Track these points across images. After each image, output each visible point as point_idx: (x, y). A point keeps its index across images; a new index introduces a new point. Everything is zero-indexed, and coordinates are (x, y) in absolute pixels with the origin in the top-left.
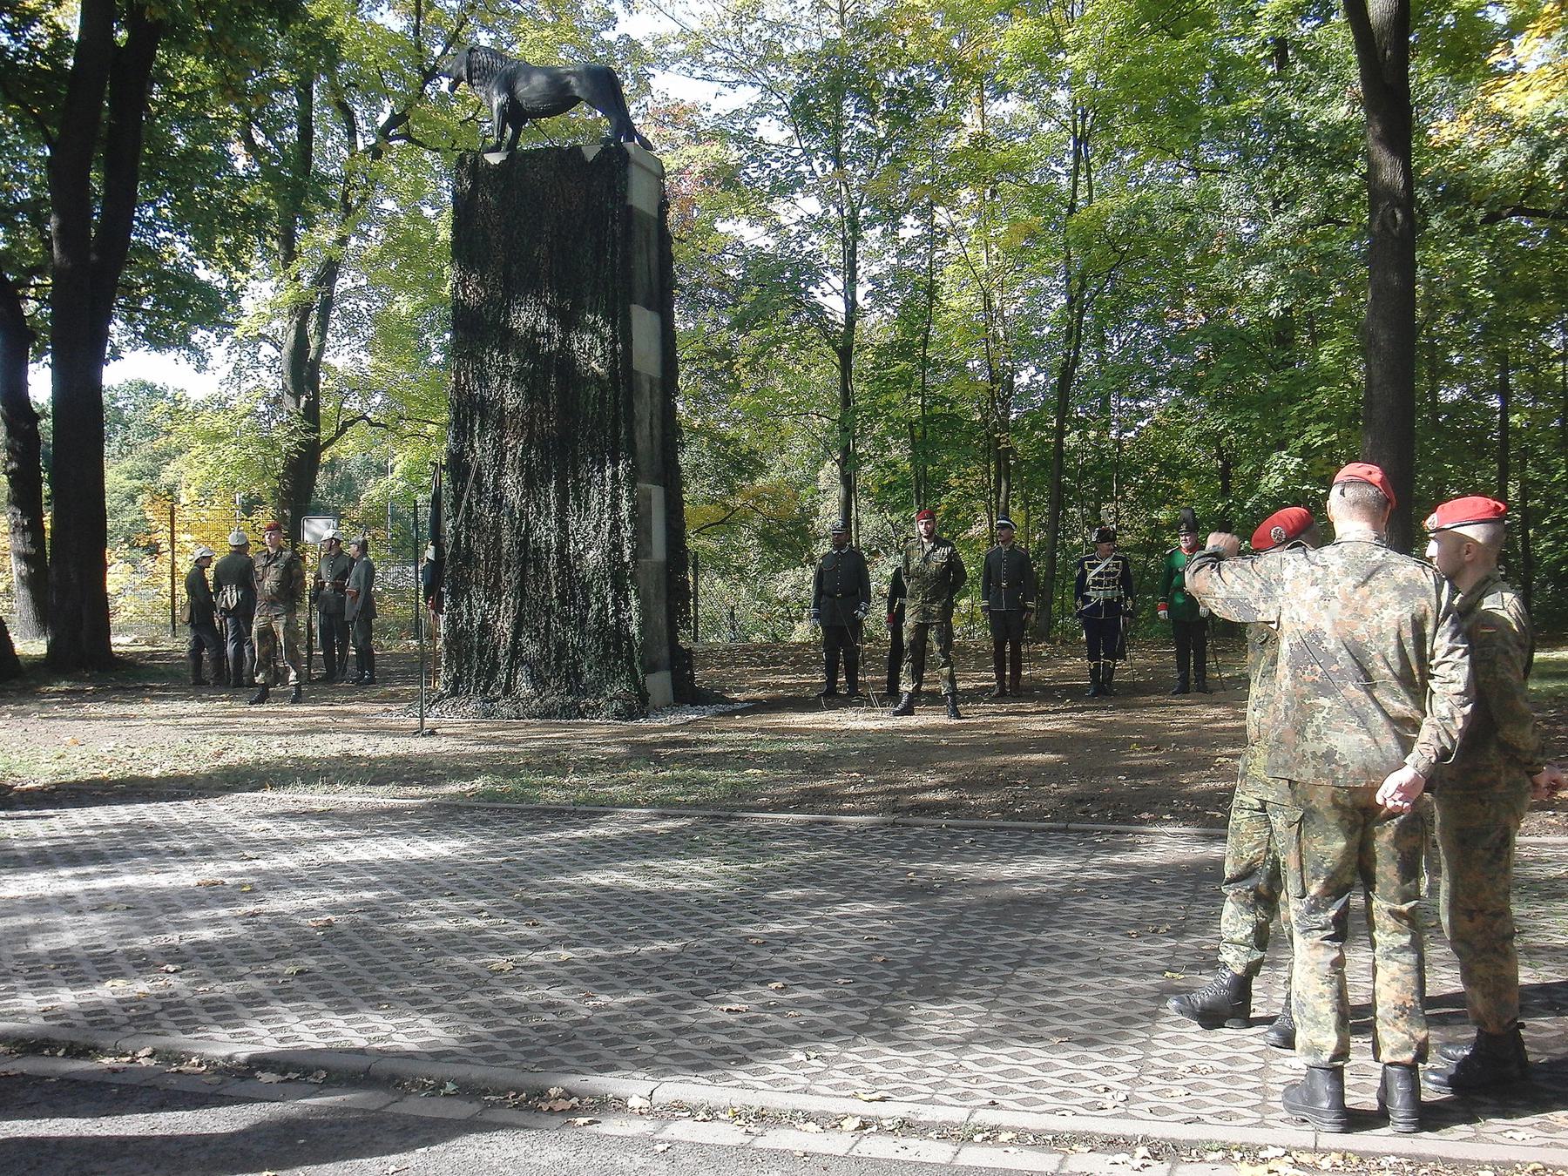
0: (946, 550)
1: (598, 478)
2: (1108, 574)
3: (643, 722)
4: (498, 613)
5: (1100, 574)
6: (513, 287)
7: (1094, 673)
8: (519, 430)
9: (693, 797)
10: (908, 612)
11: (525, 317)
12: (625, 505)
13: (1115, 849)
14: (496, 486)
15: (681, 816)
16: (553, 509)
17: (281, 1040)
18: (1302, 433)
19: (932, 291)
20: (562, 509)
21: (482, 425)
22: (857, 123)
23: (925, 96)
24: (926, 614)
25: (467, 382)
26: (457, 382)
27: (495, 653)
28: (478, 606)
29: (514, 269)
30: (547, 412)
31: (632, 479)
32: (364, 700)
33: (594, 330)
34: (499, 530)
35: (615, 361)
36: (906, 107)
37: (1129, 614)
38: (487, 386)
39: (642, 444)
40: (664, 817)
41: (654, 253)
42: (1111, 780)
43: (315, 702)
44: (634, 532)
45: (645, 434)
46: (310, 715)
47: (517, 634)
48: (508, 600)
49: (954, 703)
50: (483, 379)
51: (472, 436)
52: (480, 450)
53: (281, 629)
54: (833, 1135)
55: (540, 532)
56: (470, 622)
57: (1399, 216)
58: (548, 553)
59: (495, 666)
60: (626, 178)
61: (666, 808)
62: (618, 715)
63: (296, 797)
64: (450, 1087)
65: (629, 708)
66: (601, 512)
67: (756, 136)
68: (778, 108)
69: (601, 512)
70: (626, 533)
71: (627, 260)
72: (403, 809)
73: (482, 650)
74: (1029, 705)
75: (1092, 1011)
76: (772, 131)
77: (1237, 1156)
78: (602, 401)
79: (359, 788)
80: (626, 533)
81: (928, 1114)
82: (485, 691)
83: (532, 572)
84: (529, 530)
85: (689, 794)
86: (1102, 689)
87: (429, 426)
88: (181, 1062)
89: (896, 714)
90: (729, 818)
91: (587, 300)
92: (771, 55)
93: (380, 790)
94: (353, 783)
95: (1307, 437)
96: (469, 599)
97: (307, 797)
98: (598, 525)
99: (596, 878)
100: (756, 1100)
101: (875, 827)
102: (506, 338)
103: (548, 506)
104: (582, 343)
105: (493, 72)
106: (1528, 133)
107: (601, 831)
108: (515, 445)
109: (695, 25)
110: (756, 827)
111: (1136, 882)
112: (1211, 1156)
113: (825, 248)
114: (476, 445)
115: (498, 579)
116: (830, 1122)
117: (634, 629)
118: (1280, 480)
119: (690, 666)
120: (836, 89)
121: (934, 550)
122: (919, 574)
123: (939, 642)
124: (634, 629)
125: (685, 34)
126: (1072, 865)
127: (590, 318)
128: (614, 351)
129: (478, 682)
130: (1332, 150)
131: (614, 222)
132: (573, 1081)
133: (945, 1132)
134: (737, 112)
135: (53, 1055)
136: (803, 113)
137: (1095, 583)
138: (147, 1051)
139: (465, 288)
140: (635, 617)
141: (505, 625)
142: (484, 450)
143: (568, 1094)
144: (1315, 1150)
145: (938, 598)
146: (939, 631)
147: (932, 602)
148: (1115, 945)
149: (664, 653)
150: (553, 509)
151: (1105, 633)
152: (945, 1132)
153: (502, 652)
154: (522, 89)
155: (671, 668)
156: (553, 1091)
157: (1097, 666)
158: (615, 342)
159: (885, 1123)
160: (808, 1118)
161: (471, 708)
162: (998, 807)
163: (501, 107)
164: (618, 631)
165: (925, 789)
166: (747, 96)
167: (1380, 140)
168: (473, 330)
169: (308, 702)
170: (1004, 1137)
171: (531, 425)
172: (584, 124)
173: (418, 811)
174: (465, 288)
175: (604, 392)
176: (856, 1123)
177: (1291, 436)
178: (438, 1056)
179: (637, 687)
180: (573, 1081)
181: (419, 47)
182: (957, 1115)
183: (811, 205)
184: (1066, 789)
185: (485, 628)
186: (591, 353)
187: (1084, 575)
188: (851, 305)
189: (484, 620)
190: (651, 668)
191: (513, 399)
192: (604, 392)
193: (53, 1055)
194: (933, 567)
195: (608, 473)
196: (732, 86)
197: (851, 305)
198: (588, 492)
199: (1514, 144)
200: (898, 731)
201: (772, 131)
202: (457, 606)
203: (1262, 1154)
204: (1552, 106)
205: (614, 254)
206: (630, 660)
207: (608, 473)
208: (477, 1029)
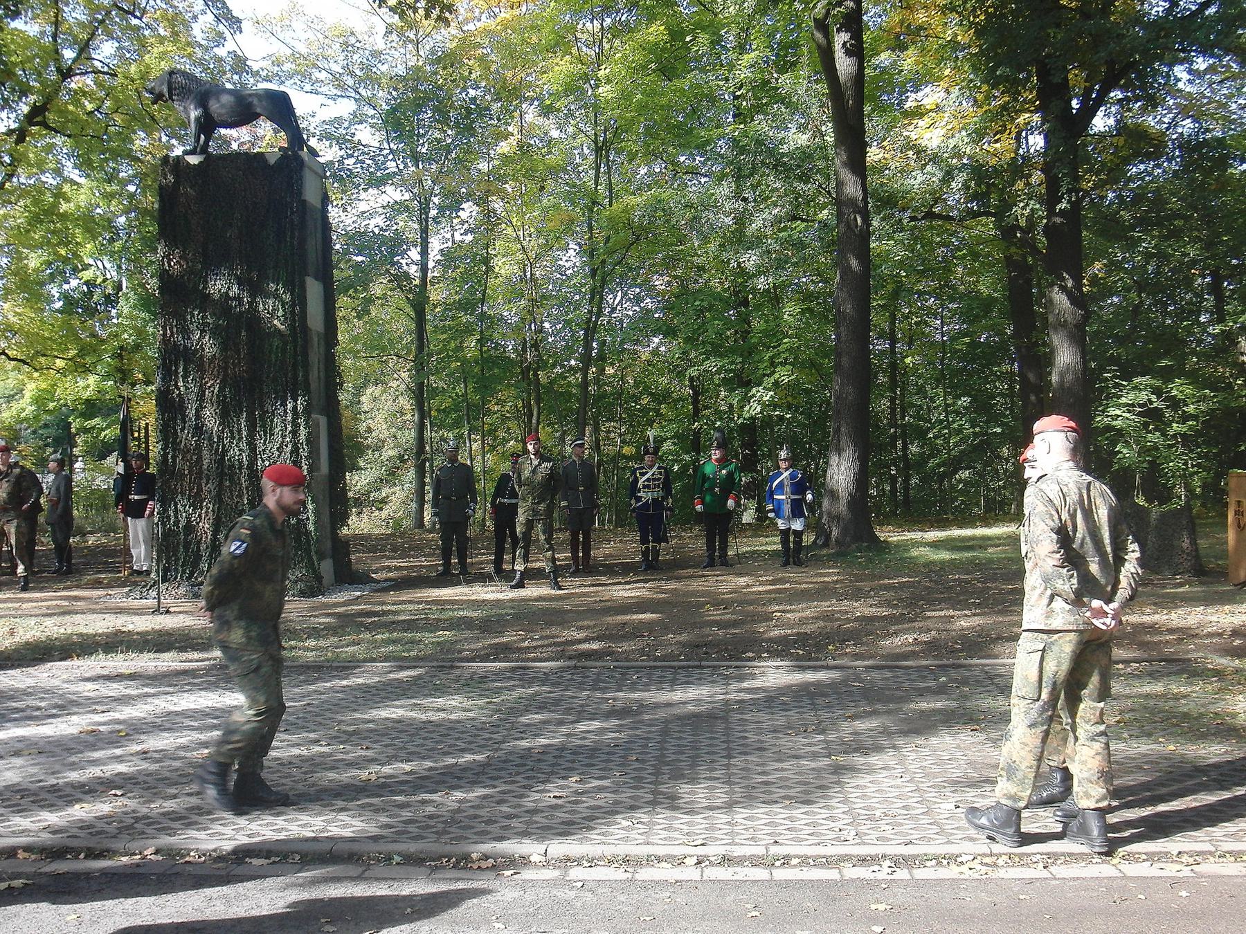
0: (548, 465)
1: (281, 411)
2: (654, 480)
3: (322, 599)
4: (200, 516)
5: (648, 480)
6: (213, 260)
7: (645, 554)
8: (215, 372)
9: (412, 653)
10: (520, 511)
11: (219, 285)
12: (303, 432)
13: (741, 678)
14: (198, 416)
15: (415, 667)
16: (244, 434)
17: (248, 836)
18: (774, 372)
19: (486, 261)
20: (251, 434)
21: (185, 370)
22: (432, 134)
23: (483, 111)
24: (535, 512)
25: (172, 335)
26: (164, 335)
27: (198, 548)
28: (183, 510)
29: (211, 247)
30: (239, 359)
31: (308, 411)
32: (78, 587)
33: (276, 296)
34: (201, 451)
35: (294, 321)
36: (469, 121)
37: (670, 509)
38: (189, 338)
39: (314, 386)
40: (401, 668)
41: (319, 235)
42: (707, 631)
43: (42, 590)
44: (310, 452)
45: (316, 374)
46: (45, 600)
47: (216, 532)
48: (208, 506)
49: (556, 578)
50: (185, 332)
51: (177, 377)
52: (183, 387)
53: (13, 530)
54: (680, 868)
55: (234, 452)
56: (177, 523)
57: (859, 220)
58: (240, 468)
59: (198, 558)
60: (301, 178)
61: (402, 663)
62: (302, 594)
63: (104, 664)
64: (397, 859)
65: (311, 588)
66: (284, 437)
67: (356, 139)
68: (373, 117)
69: (284, 437)
70: (304, 453)
71: (303, 241)
72: (194, 670)
73: (187, 545)
74: (603, 578)
75: (563, 823)
76: (367, 135)
77: (945, 862)
78: (284, 351)
79: (152, 655)
80: (304, 453)
81: (738, 851)
82: (189, 579)
83: (227, 483)
84: (225, 452)
85: (409, 651)
86: (651, 566)
87: (58, 361)
88: (183, 856)
89: (512, 587)
90: (452, 667)
91: (270, 272)
92: (370, 78)
93: (166, 656)
94: (141, 652)
95: (777, 376)
96: (176, 505)
97: (112, 664)
98: (281, 446)
99: (384, 714)
100: (622, 850)
101: (563, 669)
102: (205, 301)
103: (239, 432)
104: (265, 306)
105: (190, 91)
106: (935, 159)
107: (360, 681)
108: (213, 386)
109: (302, 49)
110: (474, 673)
111: (769, 699)
112: (928, 864)
113: (408, 226)
114: (180, 384)
115: (200, 489)
116: (680, 862)
117: (311, 527)
118: (759, 409)
119: (348, 554)
120: (418, 106)
121: (540, 464)
122: (529, 483)
123: (544, 533)
124: (311, 527)
125: (296, 57)
126: (718, 690)
127: (272, 286)
128: (293, 312)
129: (184, 572)
130: (798, 167)
131: (292, 213)
132: (487, 847)
133: (755, 862)
134: (338, 120)
135: (76, 857)
136: (397, 122)
137: (644, 487)
138: (151, 850)
139: (169, 261)
140: (312, 518)
141: (205, 526)
142: (187, 388)
143: (486, 857)
144: (991, 855)
145: (544, 500)
146: (544, 525)
147: (539, 503)
148: (785, 742)
149: (329, 544)
150: (244, 434)
151: (651, 523)
152: (755, 862)
153: (203, 547)
154: (214, 106)
155: (333, 557)
156: (474, 856)
157: (647, 548)
158: (293, 305)
159: (712, 859)
160: (659, 859)
161: (182, 590)
162: (642, 652)
163: (198, 119)
164: (298, 529)
165: (580, 642)
166: (345, 108)
167: (845, 164)
168: (175, 297)
169: (34, 589)
170: (795, 861)
171: (225, 369)
172: (263, 137)
173: (208, 671)
174: (169, 261)
175: (285, 344)
176: (694, 860)
177: (765, 375)
178: (375, 839)
179: (314, 571)
180: (487, 847)
181: (57, 51)
182: (760, 851)
183: (394, 194)
184: (679, 638)
185: (189, 528)
186: (273, 311)
187: (636, 480)
188: (424, 269)
189: (189, 522)
190: (322, 557)
191: (209, 347)
192: (285, 344)
193: (76, 857)
194: (539, 477)
195: (290, 406)
196: (333, 98)
197: (424, 269)
198: (272, 421)
199: (928, 168)
200: (523, 600)
201: (367, 135)
202: (165, 510)
203: (959, 860)
204: (952, 142)
205: (292, 238)
206: (308, 551)
207: (290, 406)
208: (384, 819)
